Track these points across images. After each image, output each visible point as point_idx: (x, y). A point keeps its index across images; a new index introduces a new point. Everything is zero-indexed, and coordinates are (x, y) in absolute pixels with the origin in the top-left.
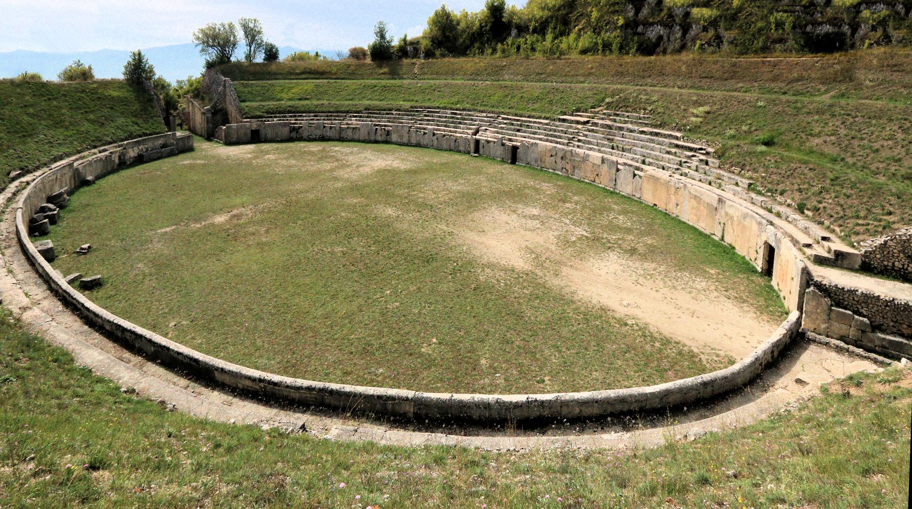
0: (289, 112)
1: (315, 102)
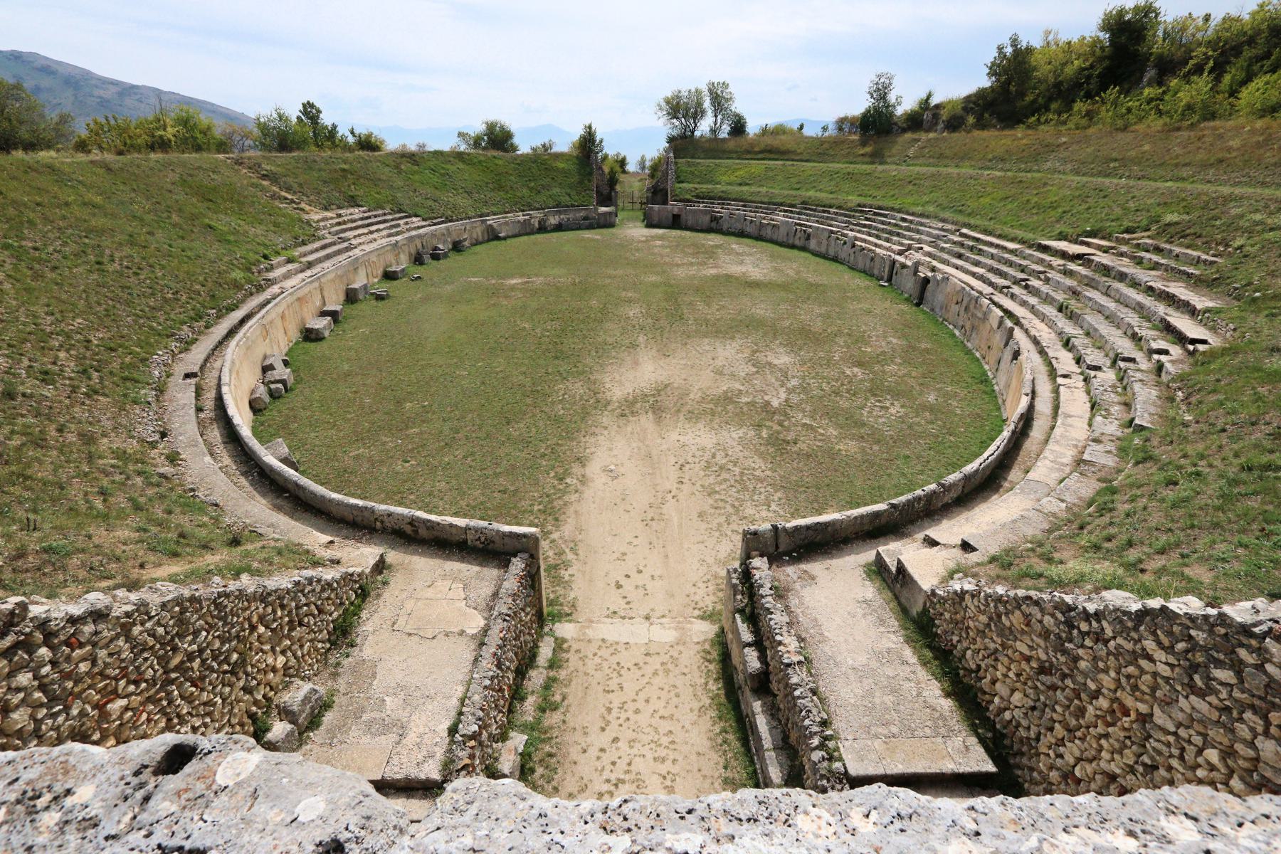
0: (720, 198)
1: (753, 189)
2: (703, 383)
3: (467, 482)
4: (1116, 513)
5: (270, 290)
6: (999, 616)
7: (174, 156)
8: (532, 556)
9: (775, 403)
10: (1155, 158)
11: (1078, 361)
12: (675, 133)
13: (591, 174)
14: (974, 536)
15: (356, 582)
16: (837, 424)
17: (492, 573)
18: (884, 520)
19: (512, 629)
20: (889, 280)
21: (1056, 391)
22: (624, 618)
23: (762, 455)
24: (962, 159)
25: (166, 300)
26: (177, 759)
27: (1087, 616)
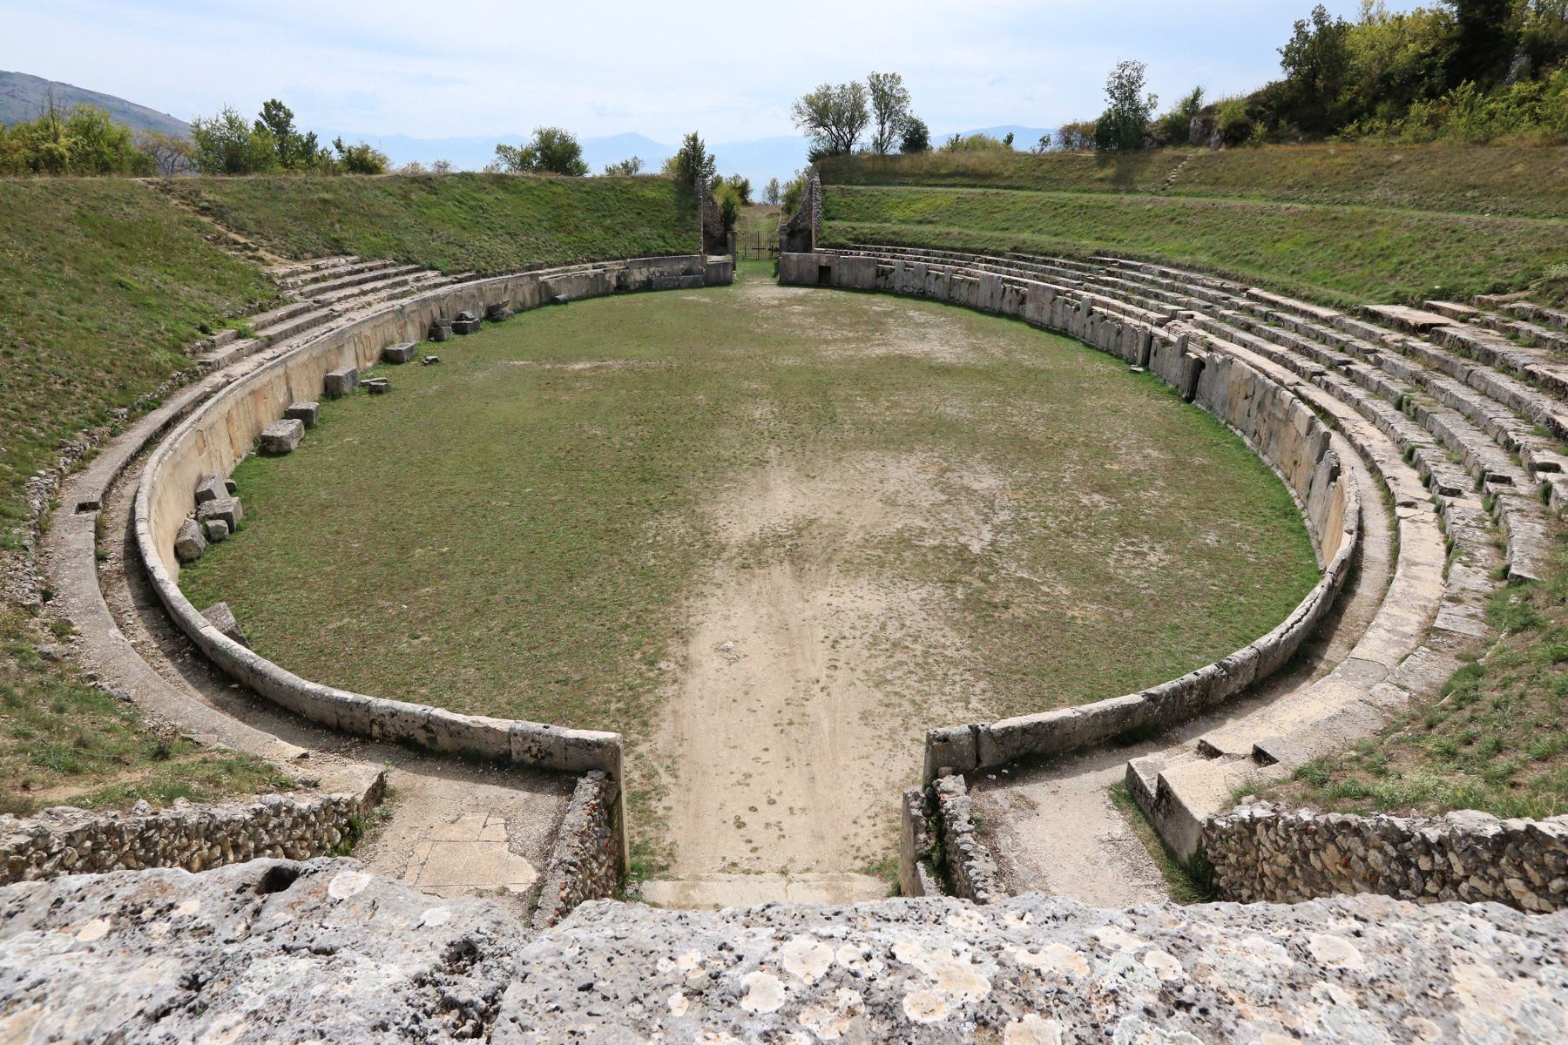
0: (890, 242)
1: (940, 229)
2: (865, 516)
3: (507, 668)
4: (1480, 705)
5: (209, 379)
6: (1306, 854)
7: (67, 179)
8: (609, 776)
9: (976, 548)
10: (1532, 184)
11: (1427, 482)
12: (821, 147)
13: (695, 207)
14: (1272, 740)
15: (342, 815)
16: (1067, 578)
17: (548, 802)
18: (1138, 720)
19: (579, 886)
20: (1145, 363)
21: (1395, 527)
22: (747, 872)
23: (955, 626)
24: (1249, 185)
25: (52, 394)
26: (277, 881)
27: (1427, 847)
